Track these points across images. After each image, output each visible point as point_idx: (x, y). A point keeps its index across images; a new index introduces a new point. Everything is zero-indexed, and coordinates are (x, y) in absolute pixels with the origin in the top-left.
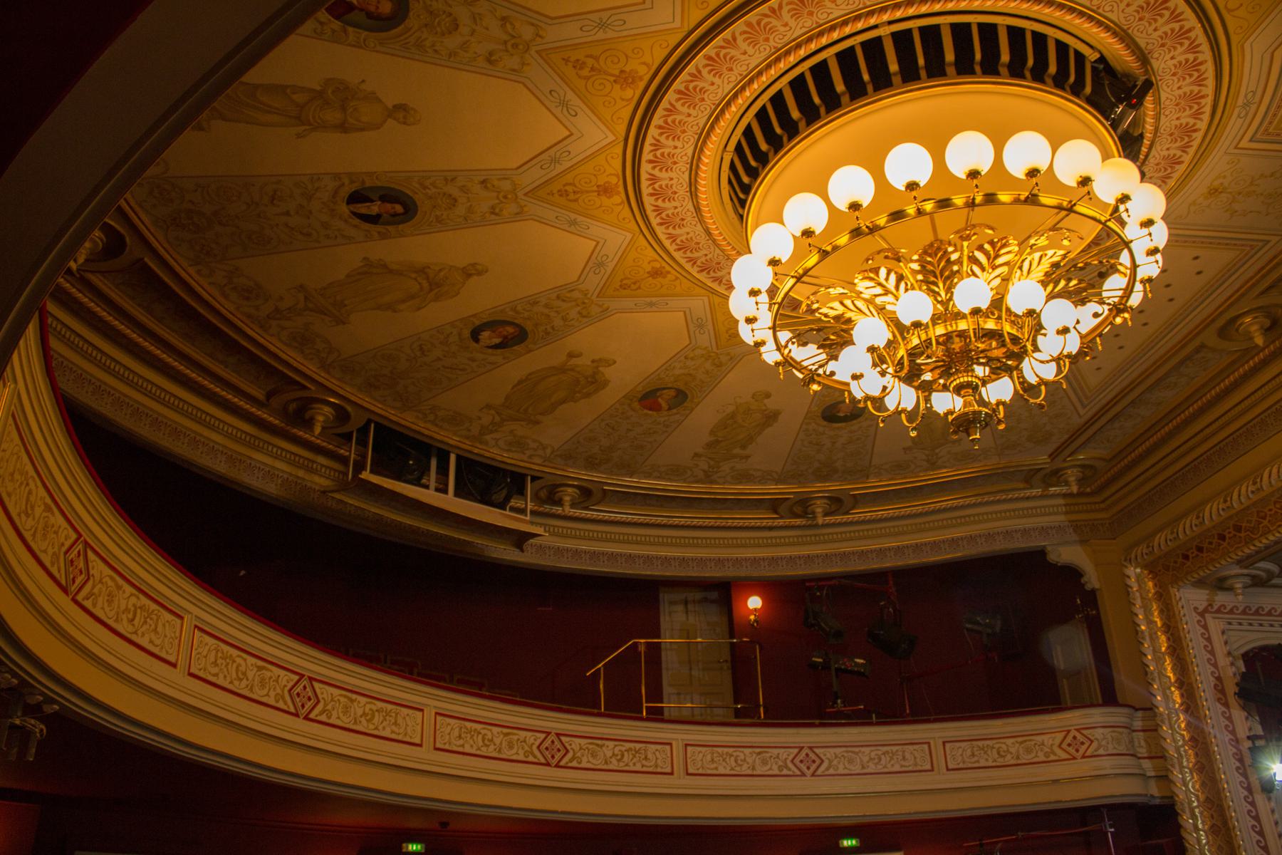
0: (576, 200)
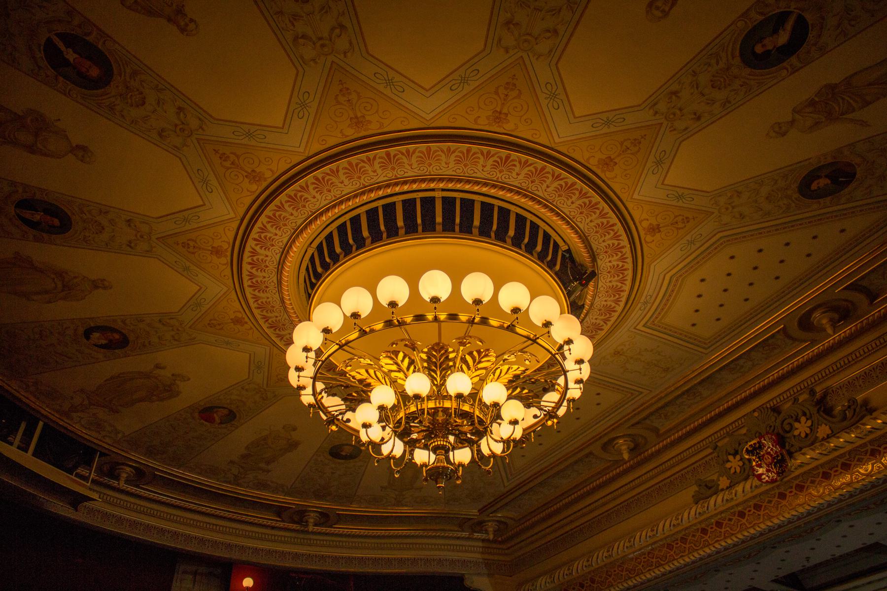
0: (193, 253)
